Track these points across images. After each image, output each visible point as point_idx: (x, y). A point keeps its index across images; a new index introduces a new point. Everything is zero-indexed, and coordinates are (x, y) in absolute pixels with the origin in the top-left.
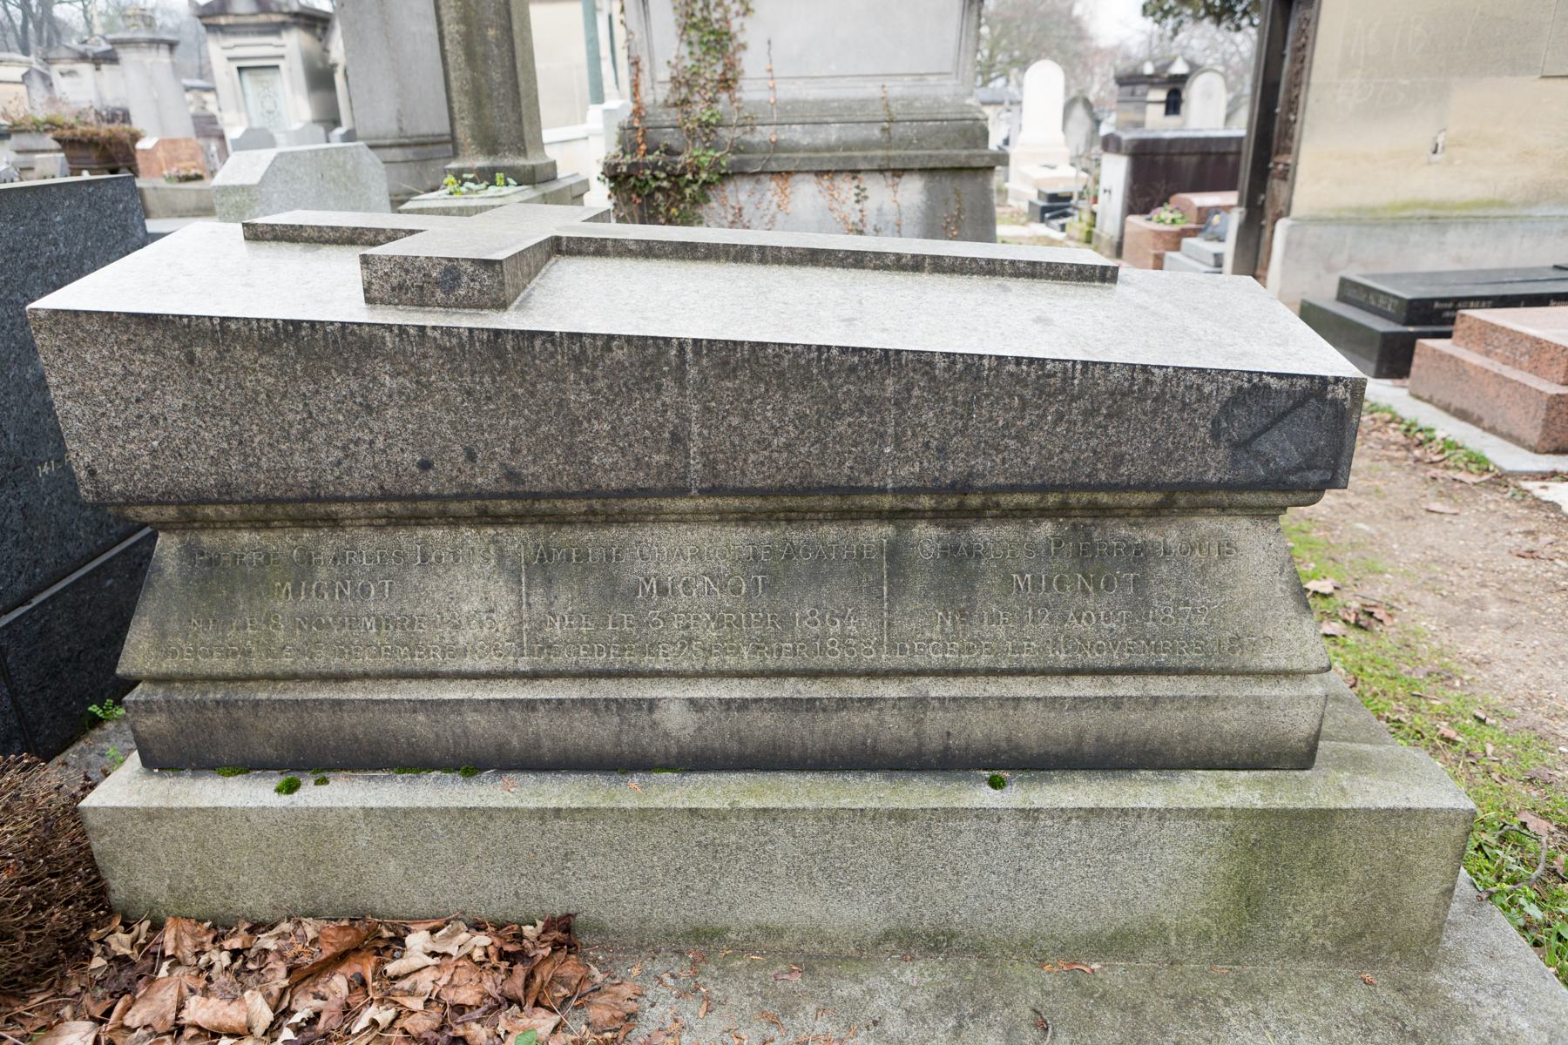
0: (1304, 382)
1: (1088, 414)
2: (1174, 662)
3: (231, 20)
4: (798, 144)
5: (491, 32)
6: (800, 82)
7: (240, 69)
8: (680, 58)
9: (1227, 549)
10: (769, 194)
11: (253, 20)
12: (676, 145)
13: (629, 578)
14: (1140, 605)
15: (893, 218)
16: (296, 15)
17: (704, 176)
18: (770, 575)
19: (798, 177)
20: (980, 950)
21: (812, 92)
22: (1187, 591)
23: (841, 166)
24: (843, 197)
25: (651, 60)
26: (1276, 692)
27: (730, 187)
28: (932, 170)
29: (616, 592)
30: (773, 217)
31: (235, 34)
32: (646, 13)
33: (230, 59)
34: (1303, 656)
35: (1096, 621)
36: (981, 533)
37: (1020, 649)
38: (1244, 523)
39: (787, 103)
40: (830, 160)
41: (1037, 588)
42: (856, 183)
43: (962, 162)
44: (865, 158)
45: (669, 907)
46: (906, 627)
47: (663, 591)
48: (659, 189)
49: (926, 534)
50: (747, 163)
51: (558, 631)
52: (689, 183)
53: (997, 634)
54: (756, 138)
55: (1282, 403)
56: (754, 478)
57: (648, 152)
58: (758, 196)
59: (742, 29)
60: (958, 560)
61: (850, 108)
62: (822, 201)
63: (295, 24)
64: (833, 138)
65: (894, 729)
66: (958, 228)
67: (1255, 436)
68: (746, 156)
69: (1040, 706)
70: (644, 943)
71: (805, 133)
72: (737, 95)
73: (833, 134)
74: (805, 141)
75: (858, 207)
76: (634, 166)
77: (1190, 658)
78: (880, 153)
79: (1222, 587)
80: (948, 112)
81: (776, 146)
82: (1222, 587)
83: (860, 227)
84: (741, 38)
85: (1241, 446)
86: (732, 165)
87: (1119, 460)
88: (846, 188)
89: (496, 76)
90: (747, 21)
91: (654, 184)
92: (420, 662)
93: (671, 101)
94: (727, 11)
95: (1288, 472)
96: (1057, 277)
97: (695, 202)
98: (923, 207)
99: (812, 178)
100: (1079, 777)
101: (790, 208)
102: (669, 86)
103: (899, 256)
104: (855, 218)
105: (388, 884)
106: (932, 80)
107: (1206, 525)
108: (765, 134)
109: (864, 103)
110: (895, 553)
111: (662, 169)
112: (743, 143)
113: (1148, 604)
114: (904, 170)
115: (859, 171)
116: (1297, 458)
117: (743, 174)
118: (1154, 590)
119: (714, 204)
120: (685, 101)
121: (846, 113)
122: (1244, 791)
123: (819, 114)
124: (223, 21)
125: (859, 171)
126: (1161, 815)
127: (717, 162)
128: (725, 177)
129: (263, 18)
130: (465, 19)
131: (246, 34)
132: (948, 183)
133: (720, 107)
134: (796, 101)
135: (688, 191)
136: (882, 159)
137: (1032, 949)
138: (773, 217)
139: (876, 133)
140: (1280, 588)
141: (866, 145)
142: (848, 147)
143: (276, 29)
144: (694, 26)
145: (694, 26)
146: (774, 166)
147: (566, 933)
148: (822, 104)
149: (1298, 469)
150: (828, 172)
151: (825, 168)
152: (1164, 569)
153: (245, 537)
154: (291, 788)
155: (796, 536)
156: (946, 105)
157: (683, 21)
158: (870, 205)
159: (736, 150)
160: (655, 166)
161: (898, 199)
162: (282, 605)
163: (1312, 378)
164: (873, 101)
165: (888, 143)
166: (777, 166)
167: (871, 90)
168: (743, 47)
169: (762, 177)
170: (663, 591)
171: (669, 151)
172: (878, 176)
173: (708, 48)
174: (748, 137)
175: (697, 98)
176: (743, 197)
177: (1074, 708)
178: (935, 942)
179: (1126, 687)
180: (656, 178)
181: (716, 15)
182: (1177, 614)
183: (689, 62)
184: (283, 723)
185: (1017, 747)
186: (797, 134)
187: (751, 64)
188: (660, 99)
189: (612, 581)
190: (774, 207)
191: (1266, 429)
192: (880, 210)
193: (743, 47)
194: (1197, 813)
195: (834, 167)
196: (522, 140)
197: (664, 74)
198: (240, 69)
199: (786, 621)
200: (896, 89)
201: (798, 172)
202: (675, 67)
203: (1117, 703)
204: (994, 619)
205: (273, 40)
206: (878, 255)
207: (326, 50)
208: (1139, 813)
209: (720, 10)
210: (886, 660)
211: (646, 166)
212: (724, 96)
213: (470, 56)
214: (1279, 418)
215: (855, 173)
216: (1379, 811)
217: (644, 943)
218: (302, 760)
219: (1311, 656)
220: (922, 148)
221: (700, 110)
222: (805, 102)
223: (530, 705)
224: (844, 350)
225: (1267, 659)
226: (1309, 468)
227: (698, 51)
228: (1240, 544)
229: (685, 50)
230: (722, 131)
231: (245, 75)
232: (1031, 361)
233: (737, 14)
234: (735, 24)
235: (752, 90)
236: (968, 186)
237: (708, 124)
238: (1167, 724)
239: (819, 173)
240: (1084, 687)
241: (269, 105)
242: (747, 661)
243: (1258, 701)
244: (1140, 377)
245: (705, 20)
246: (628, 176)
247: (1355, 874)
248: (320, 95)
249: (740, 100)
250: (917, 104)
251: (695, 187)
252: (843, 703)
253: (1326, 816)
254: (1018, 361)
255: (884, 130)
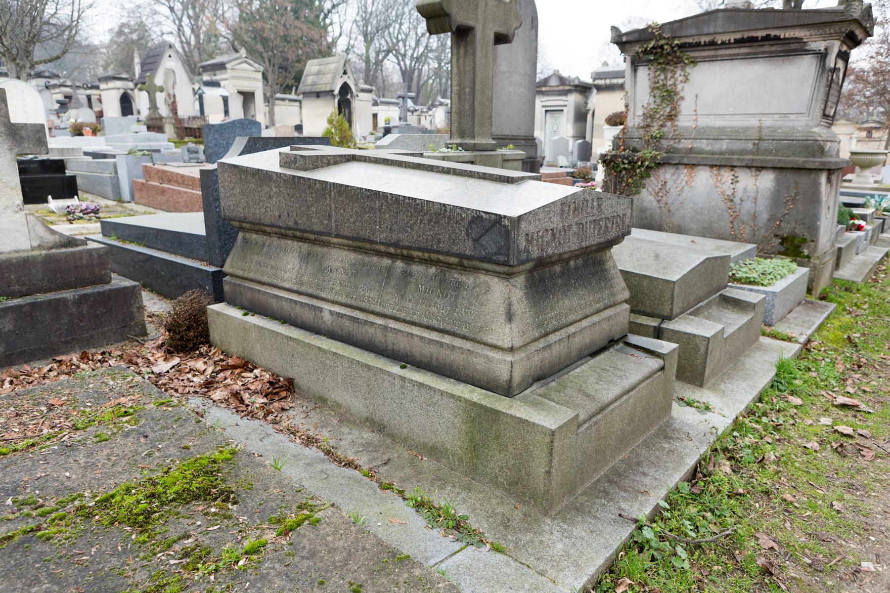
0: (493, 216)
1: (430, 221)
2: (458, 331)
3: (548, 89)
4: (703, 150)
5: (467, 90)
6: (711, 117)
7: (546, 111)
8: (649, 104)
9: (488, 289)
10: (682, 176)
11: (557, 89)
12: (638, 147)
13: (325, 265)
14: (454, 306)
15: (753, 195)
16: (576, 86)
17: (647, 163)
18: (357, 271)
19: (700, 168)
20: (391, 435)
21: (718, 123)
22: (471, 304)
23: (724, 163)
24: (724, 180)
25: (635, 105)
26: (495, 355)
27: (662, 170)
28: (781, 168)
29: (321, 270)
30: (683, 188)
31: (548, 95)
32: (635, 82)
33: (543, 106)
34: (503, 340)
35: (438, 310)
36: (416, 268)
37: (414, 314)
38: (496, 280)
39: (702, 128)
40: (717, 159)
41: (425, 292)
42: (733, 173)
43: (800, 165)
44: (738, 159)
45: (316, 389)
46: (386, 297)
47: (331, 271)
48: (625, 168)
49: (400, 264)
50: (671, 158)
51: (305, 279)
52: (639, 167)
53: (411, 308)
54: (681, 146)
55: (487, 224)
56: (346, 233)
57: (624, 150)
58: (676, 176)
59: (683, 89)
60: (406, 274)
61: (737, 132)
62: (712, 181)
63: (575, 91)
64: (724, 148)
65: (378, 337)
66: (793, 203)
67: (480, 237)
68: (671, 155)
69: (419, 340)
70: (307, 396)
71: (708, 144)
72: (676, 123)
73: (724, 145)
74: (708, 148)
75: (732, 186)
76: (615, 156)
77: (464, 331)
78: (750, 157)
79: (482, 304)
80: (798, 136)
81: (691, 150)
82: (482, 304)
83: (732, 197)
84: (682, 94)
85: (476, 241)
86: (663, 159)
87: (439, 241)
88: (727, 175)
89: (467, 107)
90: (686, 85)
91: (622, 166)
92: (275, 282)
93: (642, 125)
94: (676, 80)
95: (492, 255)
96: (492, 180)
97: (642, 177)
98: (773, 189)
99: (708, 168)
100: (429, 374)
101: (693, 184)
102: (642, 118)
103: (443, 168)
104: (729, 192)
105: (258, 352)
106: (792, 117)
107: (483, 278)
108: (686, 144)
109: (746, 129)
110: (389, 269)
111: (627, 158)
112: (673, 148)
113: (457, 307)
114: (763, 168)
115: (735, 167)
116: (495, 250)
117: (669, 164)
118: (460, 301)
119: (652, 178)
120: (648, 126)
121: (734, 134)
122: (476, 395)
123: (718, 134)
124: (544, 89)
125: (735, 167)
126: (442, 393)
127: (655, 157)
128: (659, 165)
129: (561, 88)
130: (459, 85)
131: (552, 95)
132: (791, 177)
133: (665, 129)
134: (708, 127)
135: (638, 171)
136: (749, 160)
137: (406, 441)
138: (683, 188)
139: (750, 146)
140: (502, 310)
141: (743, 152)
142: (732, 153)
143: (565, 93)
144: (658, 88)
145: (658, 88)
146: (686, 161)
147: (290, 386)
148: (721, 130)
149: (495, 254)
150: (716, 166)
151: (714, 163)
152: (465, 293)
153: (254, 236)
154: (245, 315)
155: (367, 259)
156: (798, 131)
157: (653, 86)
158: (740, 186)
159: (668, 151)
160: (624, 157)
161: (758, 183)
162: (255, 257)
163: (496, 215)
164: (752, 128)
165: (757, 151)
166: (689, 161)
167: (754, 122)
168: (682, 98)
169: (680, 166)
170: (331, 271)
171: (635, 150)
172: (747, 171)
173: (663, 99)
174: (676, 145)
175: (655, 124)
176: (668, 176)
177: (428, 343)
178: (379, 427)
179: (447, 339)
180: (623, 163)
181: (670, 83)
182: (465, 312)
183: (653, 106)
184: (248, 295)
185: (413, 355)
186: (704, 145)
187: (686, 108)
188: (636, 124)
189: (321, 265)
190: (684, 183)
191: (483, 235)
192: (745, 189)
193: (682, 98)
194: (452, 396)
195: (721, 163)
196: (473, 133)
197: (640, 112)
198: (546, 111)
199: (357, 288)
200: (768, 122)
201: (699, 165)
202: (646, 108)
203: (441, 344)
204: (410, 301)
205: (563, 98)
206: (437, 167)
207: (586, 103)
208: (435, 390)
209: (673, 80)
210: (378, 309)
211: (620, 157)
212: (669, 124)
213: (459, 98)
214: (487, 230)
215: (733, 167)
216: (515, 417)
217: (307, 396)
218: (251, 308)
219: (506, 341)
220: (778, 156)
221: (654, 131)
222: (713, 128)
223: (296, 302)
224: (366, 190)
225: (491, 339)
226: (500, 254)
227: (658, 101)
228: (492, 288)
229: (652, 100)
230: (663, 142)
231: (548, 114)
232: (413, 199)
233: (681, 82)
234: (679, 87)
235: (684, 121)
236: (804, 180)
237: (656, 138)
238: (456, 359)
239: (712, 166)
240: (434, 336)
241: (555, 128)
242: (343, 299)
243: (487, 357)
244: (443, 208)
245: (664, 85)
246: (610, 162)
247: (511, 449)
248: (579, 124)
249: (677, 126)
250: (780, 131)
251: (643, 169)
252: (366, 322)
253: (497, 413)
254: (409, 198)
255: (754, 144)
